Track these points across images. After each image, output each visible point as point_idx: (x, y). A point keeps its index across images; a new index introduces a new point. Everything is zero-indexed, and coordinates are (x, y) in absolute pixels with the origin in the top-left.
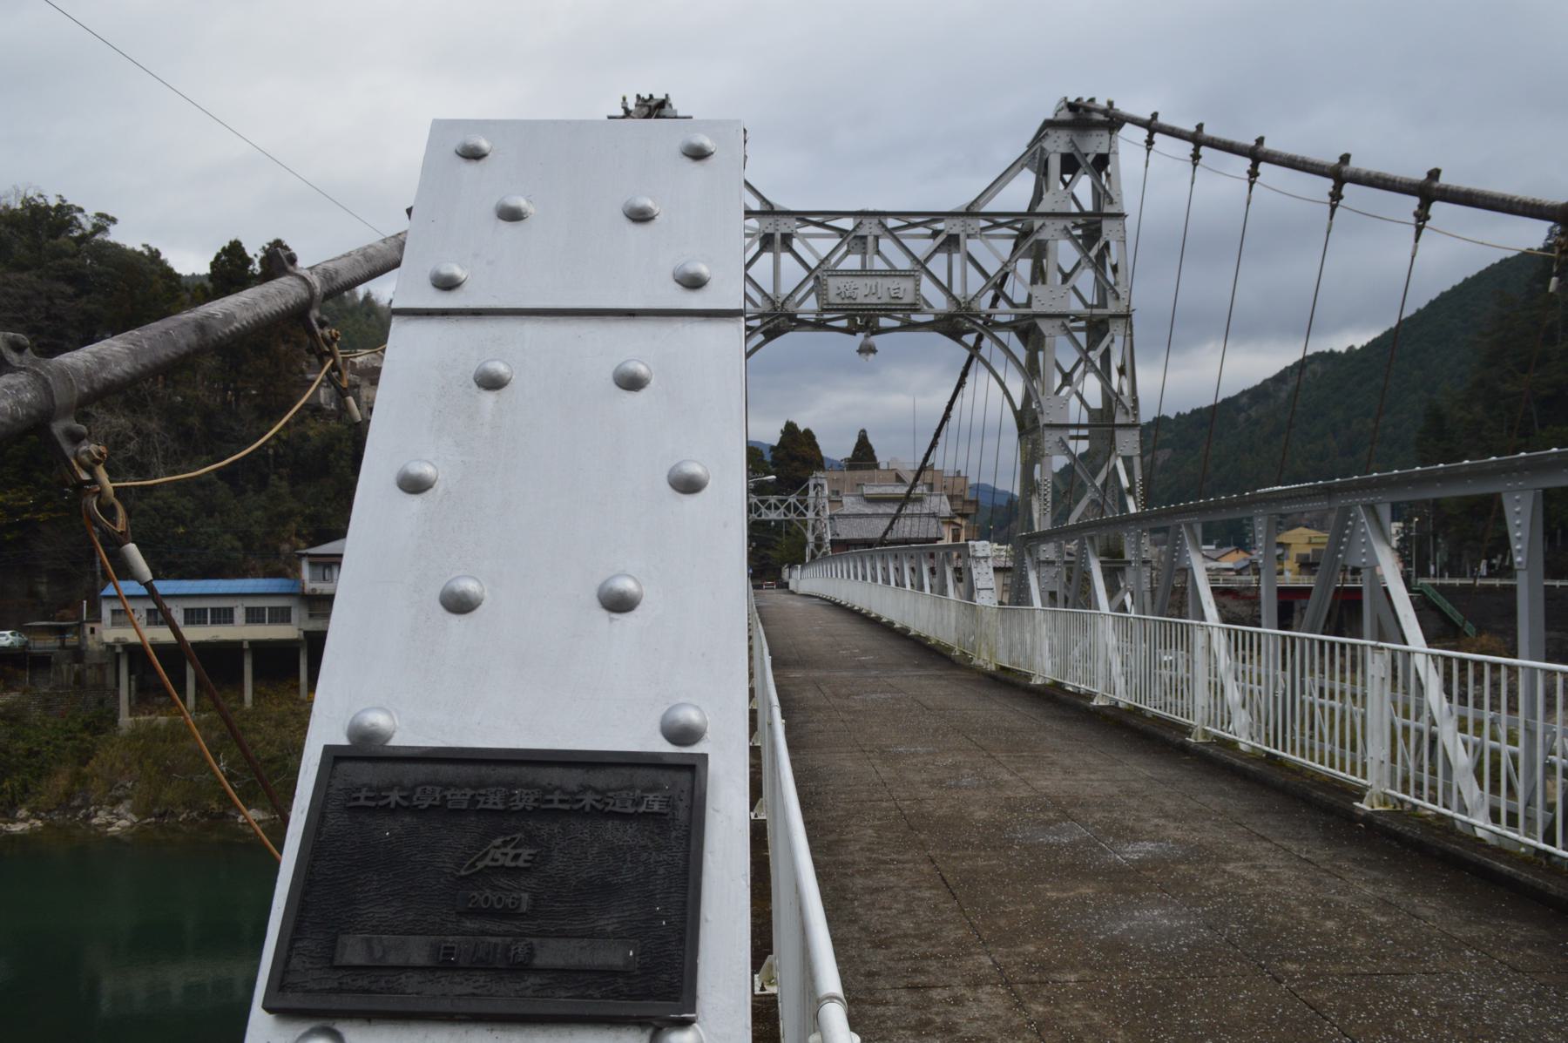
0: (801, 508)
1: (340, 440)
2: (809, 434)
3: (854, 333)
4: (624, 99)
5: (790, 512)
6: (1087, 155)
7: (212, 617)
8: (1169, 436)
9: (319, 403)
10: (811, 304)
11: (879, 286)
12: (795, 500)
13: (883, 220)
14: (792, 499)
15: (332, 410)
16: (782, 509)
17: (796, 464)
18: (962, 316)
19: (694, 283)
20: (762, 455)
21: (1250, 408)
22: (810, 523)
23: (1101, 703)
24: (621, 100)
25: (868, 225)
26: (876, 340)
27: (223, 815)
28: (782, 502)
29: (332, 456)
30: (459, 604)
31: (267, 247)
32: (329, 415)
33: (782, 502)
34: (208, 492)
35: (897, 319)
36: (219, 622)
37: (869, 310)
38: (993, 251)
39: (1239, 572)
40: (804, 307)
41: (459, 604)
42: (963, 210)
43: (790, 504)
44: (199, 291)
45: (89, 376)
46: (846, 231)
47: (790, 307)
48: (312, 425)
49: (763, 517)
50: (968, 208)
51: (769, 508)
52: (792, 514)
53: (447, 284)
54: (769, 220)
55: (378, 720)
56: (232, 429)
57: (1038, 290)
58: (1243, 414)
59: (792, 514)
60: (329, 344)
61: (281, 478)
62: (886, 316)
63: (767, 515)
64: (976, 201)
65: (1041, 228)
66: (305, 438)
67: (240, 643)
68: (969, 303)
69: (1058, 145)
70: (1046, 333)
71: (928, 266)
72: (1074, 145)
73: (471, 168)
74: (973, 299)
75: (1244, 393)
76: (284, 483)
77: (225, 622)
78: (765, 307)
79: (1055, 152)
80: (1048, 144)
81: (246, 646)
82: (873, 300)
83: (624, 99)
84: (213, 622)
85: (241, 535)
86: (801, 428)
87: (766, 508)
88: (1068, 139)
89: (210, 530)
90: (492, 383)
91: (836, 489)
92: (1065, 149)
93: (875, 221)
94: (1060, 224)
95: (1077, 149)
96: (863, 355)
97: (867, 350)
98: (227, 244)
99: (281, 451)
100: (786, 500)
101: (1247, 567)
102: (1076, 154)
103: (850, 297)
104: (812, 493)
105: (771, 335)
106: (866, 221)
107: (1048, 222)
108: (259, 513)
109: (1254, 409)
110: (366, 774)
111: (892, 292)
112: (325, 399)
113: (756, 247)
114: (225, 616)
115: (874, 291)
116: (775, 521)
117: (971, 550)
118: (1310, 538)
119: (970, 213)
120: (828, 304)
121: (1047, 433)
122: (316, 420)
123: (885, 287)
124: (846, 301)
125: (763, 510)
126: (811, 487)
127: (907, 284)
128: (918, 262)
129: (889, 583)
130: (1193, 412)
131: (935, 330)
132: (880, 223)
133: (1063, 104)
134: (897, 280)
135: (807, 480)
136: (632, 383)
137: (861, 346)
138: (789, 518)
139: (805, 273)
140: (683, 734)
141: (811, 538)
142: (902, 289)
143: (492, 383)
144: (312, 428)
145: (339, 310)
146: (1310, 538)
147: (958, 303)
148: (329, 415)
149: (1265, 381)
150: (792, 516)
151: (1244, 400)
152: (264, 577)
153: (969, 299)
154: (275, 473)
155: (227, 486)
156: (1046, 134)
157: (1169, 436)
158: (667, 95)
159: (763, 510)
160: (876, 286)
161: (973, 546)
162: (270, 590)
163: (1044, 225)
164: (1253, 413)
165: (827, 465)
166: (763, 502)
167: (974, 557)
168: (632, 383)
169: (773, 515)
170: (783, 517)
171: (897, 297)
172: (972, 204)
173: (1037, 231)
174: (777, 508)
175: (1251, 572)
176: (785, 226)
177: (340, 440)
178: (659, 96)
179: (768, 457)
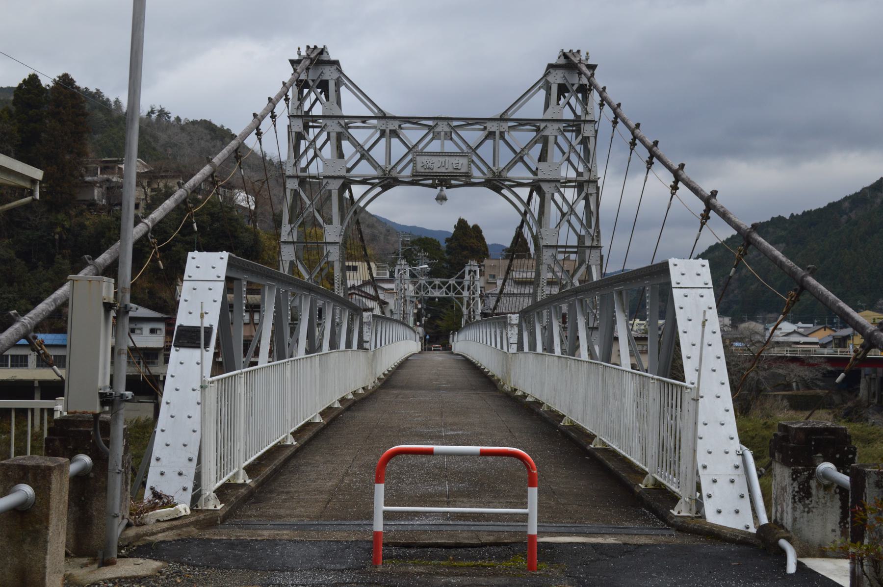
0: (459, 288)
1: (109, 229)
2: (477, 229)
3: (436, 188)
4: (299, 49)
5: (450, 292)
6: (573, 85)
7: (11, 362)
8: (783, 233)
9: (94, 200)
10: (408, 172)
11: (447, 162)
12: (454, 282)
13: (450, 123)
14: (452, 281)
15: (103, 205)
16: (444, 289)
17: (465, 253)
18: (495, 180)
19: (219, 277)
20: (438, 245)
21: (851, 211)
22: (465, 300)
23: (530, 400)
24: (297, 50)
25: (441, 126)
26: (447, 192)
28: (444, 283)
29: (103, 240)
30: (190, 313)
31: (57, 79)
32: (101, 209)
33: (444, 283)
34: (9, 267)
35: (461, 181)
36: (17, 366)
37: (441, 176)
38: (521, 138)
39: (824, 346)
40: (403, 174)
41: (190, 313)
42: (498, 117)
43: (450, 285)
44: (5, 112)
45: (103, 265)
46: (431, 126)
47: (394, 174)
48: (88, 217)
49: (430, 295)
50: (501, 116)
51: (434, 288)
52: (452, 293)
53: (190, 277)
54: (384, 121)
55: (182, 324)
56: (29, 219)
57: (542, 166)
58: (845, 217)
59: (452, 293)
60: (154, 244)
61: (64, 257)
62: (453, 179)
63: (432, 293)
64: (506, 112)
65: (544, 128)
66: (83, 226)
67: (31, 382)
68: (500, 173)
69: (557, 78)
70: (546, 191)
71: (478, 151)
72: (566, 79)
73: (193, 260)
74: (502, 170)
75: (846, 198)
76: (67, 261)
77: (21, 366)
78: (380, 174)
79: (554, 83)
80: (550, 78)
81: (36, 384)
82: (443, 170)
83: (299, 49)
84: (12, 366)
85: (33, 300)
86: (471, 224)
87: (432, 288)
88: (562, 75)
89: (10, 296)
90: (195, 289)
91: (493, 273)
92: (561, 81)
93: (445, 123)
94: (556, 126)
95: (567, 81)
96: (439, 201)
97: (441, 199)
98: (27, 77)
99: (64, 237)
100: (447, 282)
101: (831, 342)
102: (567, 84)
103: (429, 168)
104: (467, 277)
105: (386, 187)
106: (440, 123)
108: (47, 284)
109: (854, 212)
110: (181, 328)
111: (454, 165)
112: (98, 196)
113: (378, 135)
114: (21, 361)
115: (443, 165)
116: (438, 298)
117: (508, 320)
118: (874, 319)
119: (502, 119)
120: (416, 172)
121: (545, 250)
122: (91, 213)
123: (450, 163)
124: (427, 171)
125: (430, 289)
126: (467, 272)
127: (463, 161)
128: (471, 148)
129: (552, 350)
130: (804, 213)
131: (485, 187)
132: (449, 124)
133: (561, 53)
134: (457, 158)
135: (464, 266)
136: (210, 289)
137: (438, 196)
138: (449, 295)
139: (406, 150)
140: (211, 326)
141: (465, 310)
142: (460, 164)
143: (195, 289)
144: (88, 219)
145: (106, 120)
146: (874, 319)
147: (494, 173)
148: (101, 209)
149: (864, 189)
150: (452, 294)
151: (847, 204)
152: (50, 333)
153: (500, 169)
154: (59, 254)
155: (24, 262)
156: (549, 72)
157: (783, 233)
158: (324, 46)
159: (430, 289)
160: (445, 162)
161: (510, 317)
162: (55, 343)
163: (546, 126)
164: (853, 215)
165: (490, 252)
166: (430, 283)
167: (510, 324)
168: (210, 289)
169: (437, 294)
170: (444, 295)
171: (457, 169)
172: (504, 113)
173: (542, 130)
174: (440, 288)
175: (834, 345)
176: (393, 126)
177: (109, 229)
178: (320, 46)
179: (443, 245)
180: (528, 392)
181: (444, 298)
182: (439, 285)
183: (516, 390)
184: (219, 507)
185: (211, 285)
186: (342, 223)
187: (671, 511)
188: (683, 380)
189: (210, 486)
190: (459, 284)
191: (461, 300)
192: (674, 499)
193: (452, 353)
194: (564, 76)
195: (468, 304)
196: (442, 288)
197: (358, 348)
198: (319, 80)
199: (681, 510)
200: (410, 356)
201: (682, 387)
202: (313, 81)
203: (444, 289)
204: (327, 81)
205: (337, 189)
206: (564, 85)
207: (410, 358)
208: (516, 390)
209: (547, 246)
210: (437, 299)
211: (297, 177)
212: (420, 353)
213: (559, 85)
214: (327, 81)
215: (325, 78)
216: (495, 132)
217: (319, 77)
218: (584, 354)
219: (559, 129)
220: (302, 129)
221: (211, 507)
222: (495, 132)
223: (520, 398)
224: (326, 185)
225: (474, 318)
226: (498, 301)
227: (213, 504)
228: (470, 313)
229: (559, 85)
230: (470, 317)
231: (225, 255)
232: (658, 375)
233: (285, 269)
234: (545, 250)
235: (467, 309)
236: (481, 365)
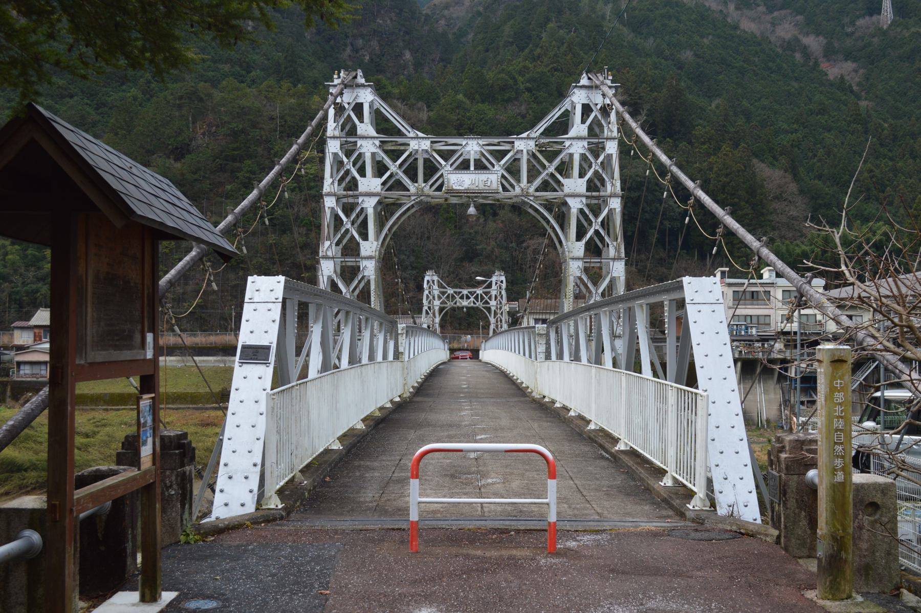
6: (597, 104)
16: (472, 299)
27: (459, 130)
43: (463, 295)
51: (462, 298)
72: (590, 99)
95: (591, 101)
104: (494, 287)
107: (574, 142)
116: (467, 308)
150: (479, 304)
163: (571, 144)
169: (465, 303)
170: (472, 304)
174: (468, 298)
180: (546, 394)
181: (472, 308)
182: (467, 295)
183: (544, 397)
184: (280, 506)
185: (270, 306)
186: (377, 239)
187: (688, 505)
188: (697, 388)
189: (275, 484)
190: (486, 293)
191: (489, 309)
192: (690, 494)
193: (480, 361)
194: (588, 96)
195: (496, 314)
196: (470, 298)
197: (394, 359)
198: (354, 103)
199: (696, 504)
200: (440, 365)
201: (696, 394)
202: (349, 103)
203: (472, 299)
204: (362, 104)
205: (373, 206)
206: (588, 105)
207: (440, 367)
208: (544, 397)
209: (573, 259)
210: (465, 309)
211: (334, 195)
212: (449, 361)
213: (583, 105)
214: (362, 104)
215: (359, 101)
216: (522, 151)
217: (354, 100)
218: (608, 363)
219: (584, 146)
220: (339, 148)
221: (273, 506)
222: (522, 151)
223: (548, 405)
224: (362, 202)
225: (501, 327)
226: (415, 138)
227: (275, 503)
228: (497, 322)
229: (583, 105)
230: (497, 326)
231: (282, 278)
232: (675, 383)
233: (323, 283)
234: (571, 263)
235: (494, 318)
236: (522, 383)
